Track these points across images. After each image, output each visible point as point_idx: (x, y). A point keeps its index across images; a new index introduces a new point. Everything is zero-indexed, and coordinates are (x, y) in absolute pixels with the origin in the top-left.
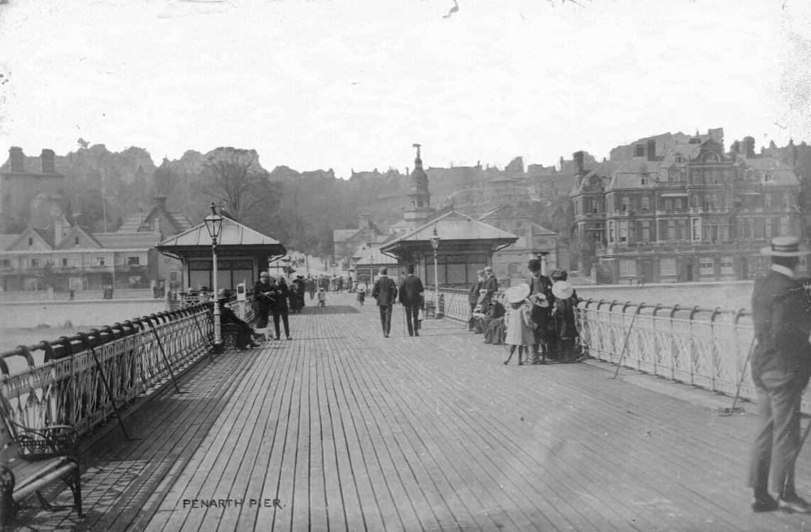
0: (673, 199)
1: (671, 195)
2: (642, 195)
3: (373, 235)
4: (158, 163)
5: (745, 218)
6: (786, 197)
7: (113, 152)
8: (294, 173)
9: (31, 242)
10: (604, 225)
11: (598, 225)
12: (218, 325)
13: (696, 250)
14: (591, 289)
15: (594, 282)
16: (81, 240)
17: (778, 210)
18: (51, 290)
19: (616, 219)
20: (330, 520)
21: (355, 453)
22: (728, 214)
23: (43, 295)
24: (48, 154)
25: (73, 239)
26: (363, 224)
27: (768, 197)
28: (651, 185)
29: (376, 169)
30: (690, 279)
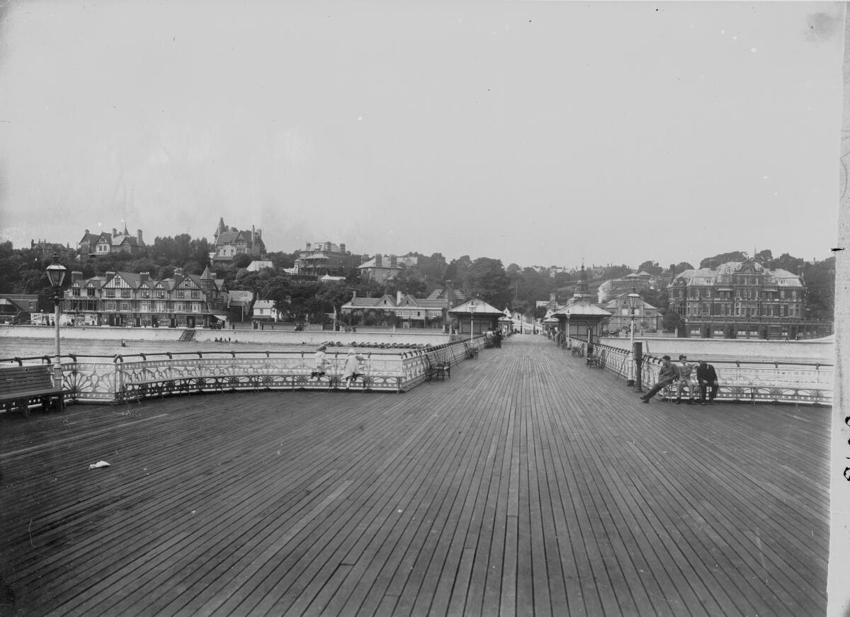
0: (725, 292)
1: (723, 290)
2: (792, 290)
3: (557, 305)
4: (448, 262)
5: (785, 305)
6: (794, 293)
7: (430, 255)
8: (285, 255)
9: (385, 302)
10: (685, 305)
11: (681, 305)
12: (268, 372)
13: (736, 321)
14: (674, 340)
15: (676, 336)
16: (410, 302)
17: (789, 300)
18: (394, 327)
19: (691, 301)
20: (825, 346)
21: (218, 513)
22: (757, 302)
23: (391, 330)
24: (349, 252)
25: (406, 302)
26: (553, 298)
27: (782, 294)
28: (712, 284)
29: (87, 231)
30: (708, 337)
